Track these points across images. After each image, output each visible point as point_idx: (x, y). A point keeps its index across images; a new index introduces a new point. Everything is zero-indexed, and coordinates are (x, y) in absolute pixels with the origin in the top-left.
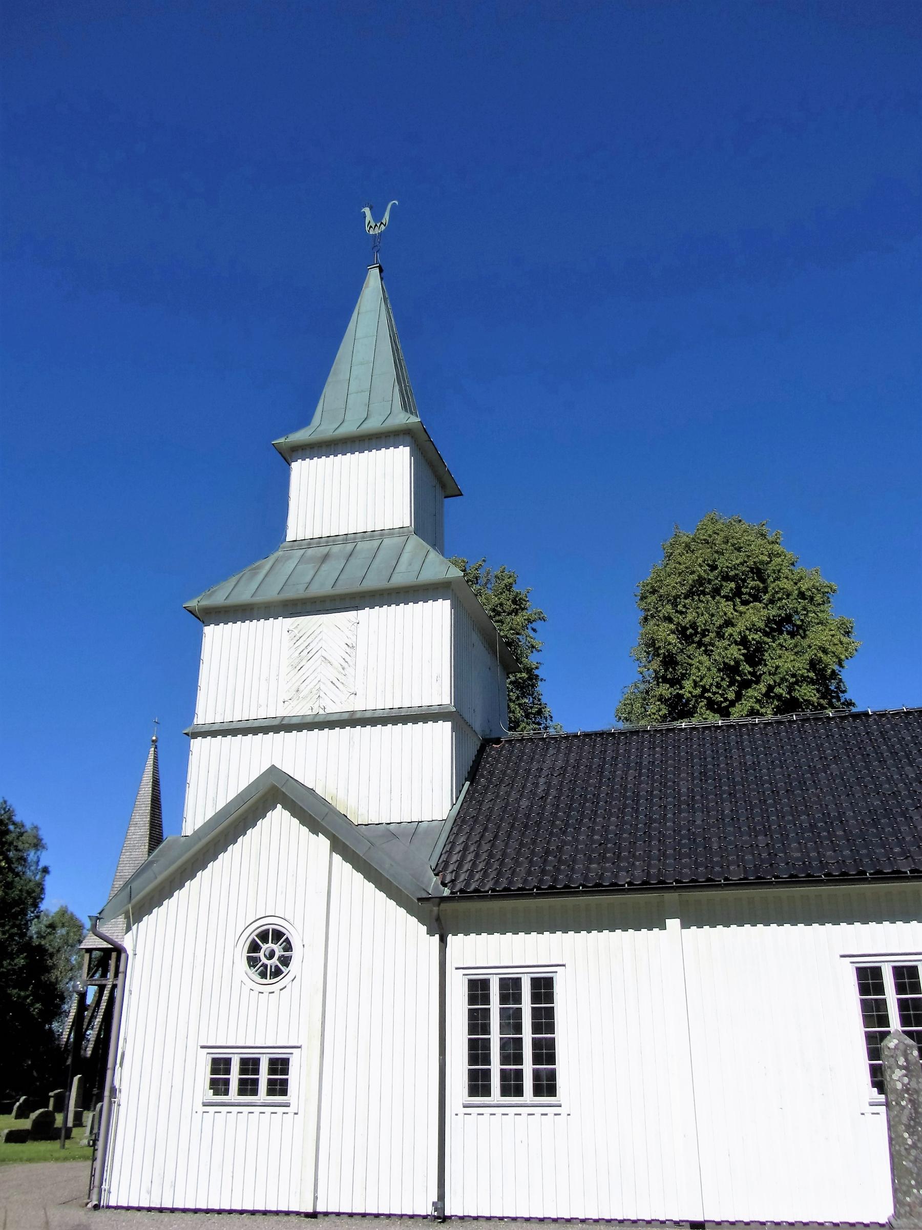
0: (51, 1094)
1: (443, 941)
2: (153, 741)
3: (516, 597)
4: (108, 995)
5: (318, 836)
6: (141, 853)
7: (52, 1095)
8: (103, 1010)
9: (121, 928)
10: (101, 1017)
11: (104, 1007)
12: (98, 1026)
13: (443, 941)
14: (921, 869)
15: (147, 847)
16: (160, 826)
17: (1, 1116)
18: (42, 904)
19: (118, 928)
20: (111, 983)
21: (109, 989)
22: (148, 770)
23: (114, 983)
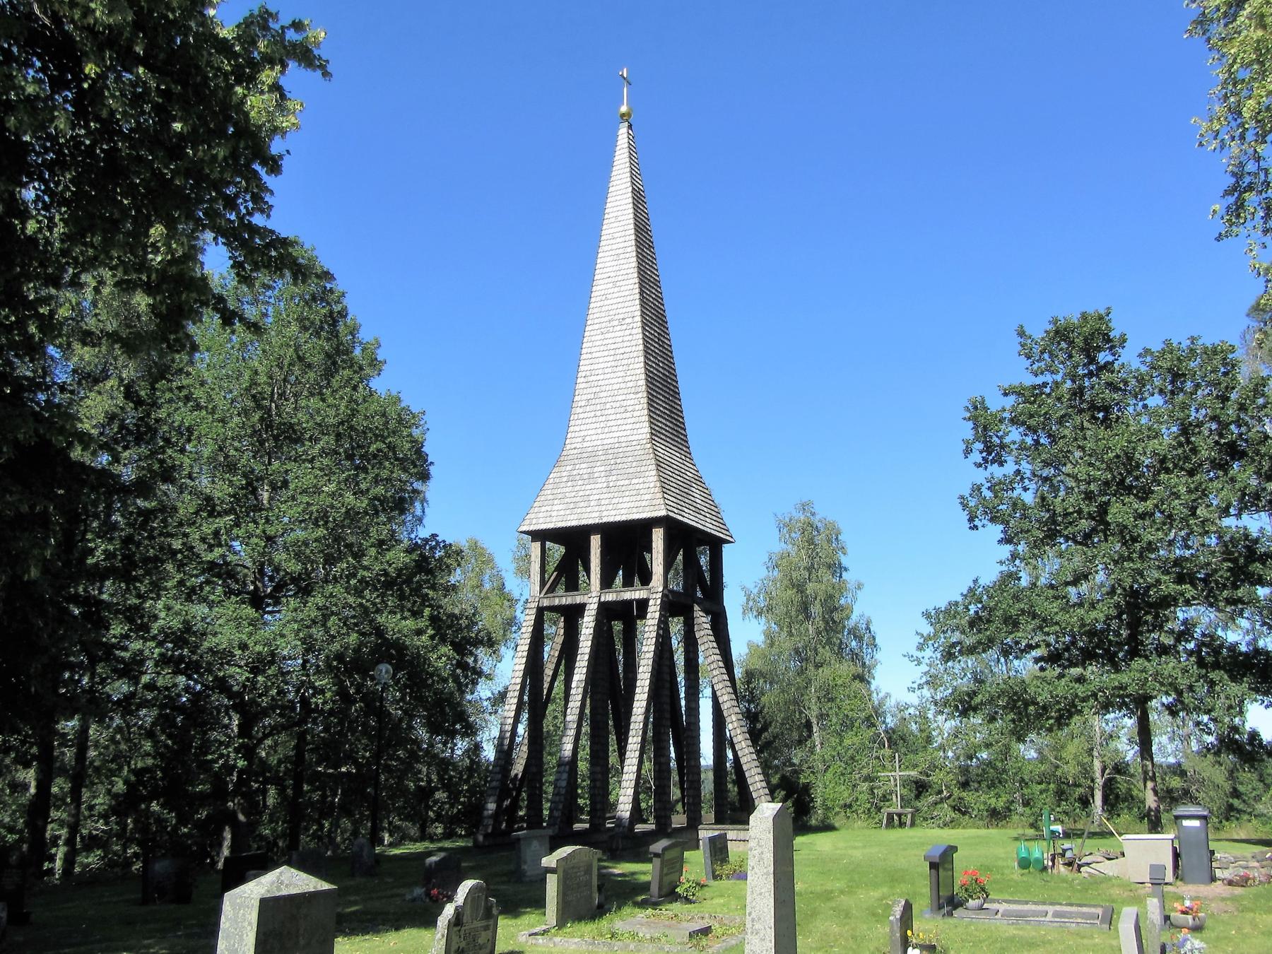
0: (549, 861)
2: (623, 115)
3: (976, 676)
4: (592, 624)
5: (927, 615)
6: (627, 332)
7: (554, 865)
8: (587, 657)
9: (605, 485)
10: (585, 670)
11: (588, 650)
12: (581, 690)
14: (803, 943)
15: (638, 319)
16: (657, 283)
17: (222, 945)
18: (1029, 951)
19: (597, 486)
20: (596, 600)
21: (594, 612)
22: (619, 177)
23: (602, 600)
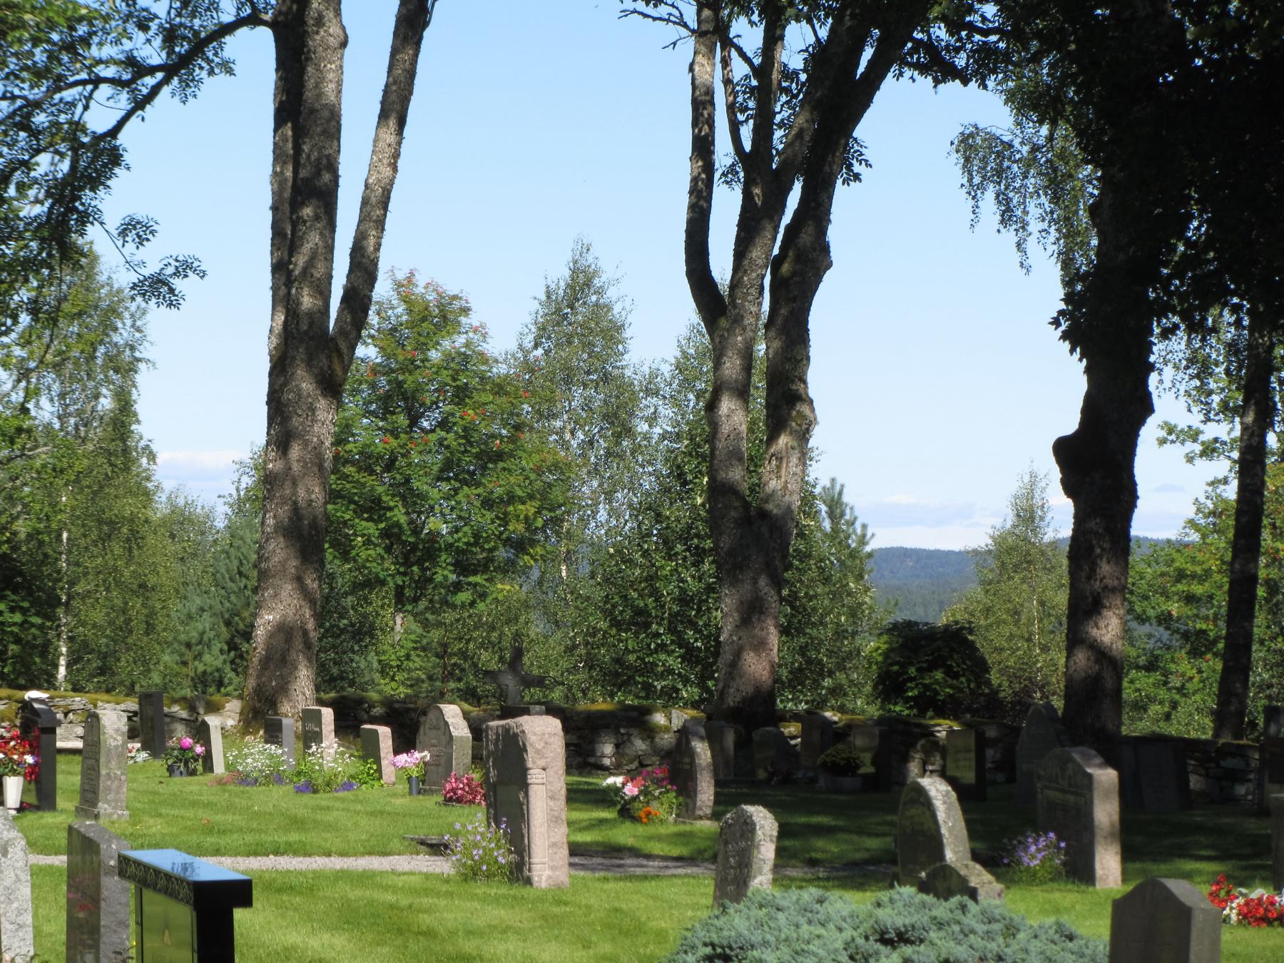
1: (114, 132)
13: (114, 132)
